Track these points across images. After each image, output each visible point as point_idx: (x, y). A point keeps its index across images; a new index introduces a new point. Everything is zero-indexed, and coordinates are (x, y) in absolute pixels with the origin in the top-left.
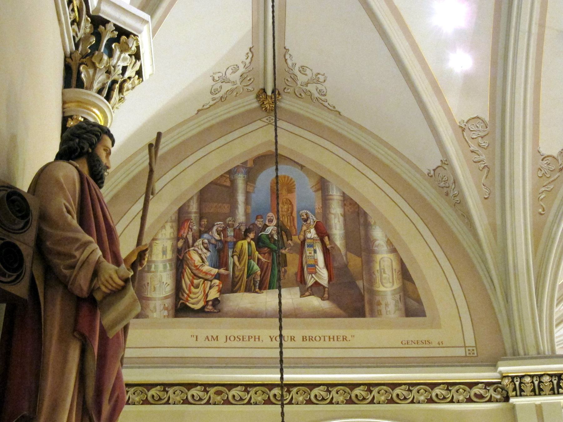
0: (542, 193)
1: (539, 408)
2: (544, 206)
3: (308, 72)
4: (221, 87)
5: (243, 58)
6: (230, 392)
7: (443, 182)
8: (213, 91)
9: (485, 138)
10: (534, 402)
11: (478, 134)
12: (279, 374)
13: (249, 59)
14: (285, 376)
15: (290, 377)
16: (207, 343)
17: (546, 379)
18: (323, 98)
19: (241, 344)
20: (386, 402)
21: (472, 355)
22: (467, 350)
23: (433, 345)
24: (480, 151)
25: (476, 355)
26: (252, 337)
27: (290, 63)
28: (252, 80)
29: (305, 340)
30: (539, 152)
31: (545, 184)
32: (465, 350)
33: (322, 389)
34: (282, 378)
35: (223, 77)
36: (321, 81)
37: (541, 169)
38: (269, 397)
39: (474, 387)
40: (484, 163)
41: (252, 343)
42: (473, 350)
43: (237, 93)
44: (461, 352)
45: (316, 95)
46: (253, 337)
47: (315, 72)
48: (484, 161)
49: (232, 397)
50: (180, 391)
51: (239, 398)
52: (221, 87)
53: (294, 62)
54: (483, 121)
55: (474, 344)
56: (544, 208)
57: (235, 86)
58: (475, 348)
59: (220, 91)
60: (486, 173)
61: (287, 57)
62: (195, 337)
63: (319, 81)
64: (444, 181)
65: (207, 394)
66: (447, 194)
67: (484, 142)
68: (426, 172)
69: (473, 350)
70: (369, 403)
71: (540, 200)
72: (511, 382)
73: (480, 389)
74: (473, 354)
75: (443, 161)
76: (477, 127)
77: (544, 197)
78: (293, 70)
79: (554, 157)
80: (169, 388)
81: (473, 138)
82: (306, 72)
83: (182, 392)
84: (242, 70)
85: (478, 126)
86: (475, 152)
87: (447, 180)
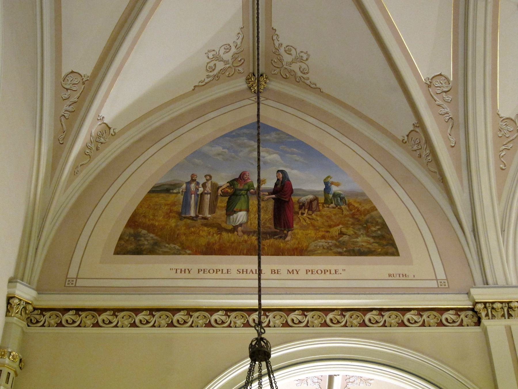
0: (502, 151)
2: (506, 163)
3: (293, 52)
4: (215, 65)
6: (212, 317)
7: (416, 145)
13: (240, 40)
14: (263, 301)
15: (267, 302)
18: (304, 76)
20: (358, 326)
21: (443, 287)
22: (439, 283)
24: (445, 105)
25: (447, 286)
26: (220, 270)
28: (243, 61)
29: (273, 273)
30: (499, 115)
31: (504, 144)
32: (437, 282)
34: (260, 304)
36: (304, 60)
37: (501, 130)
39: (446, 313)
40: (449, 115)
42: (445, 282)
43: (229, 74)
44: (434, 284)
49: (66, 322)
51: (221, 321)
52: (215, 65)
53: (280, 42)
54: (446, 78)
55: (445, 278)
56: (505, 164)
57: (228, 66)
58: (446, 281)
60: (451, 124)
61: (275, 38)
64: (417, 144)
66: (420, 156)
68: (401, 138)
71: (501, 157)
74: (445, 285)
75: (415, 124)
76: (441, 83)
77: (505, 154)
78: (280, 50)
79: (512, 119)
80: (155, 312)
82: (291, 52)
83: (168, 317)
84: (233, 50)
87: (420, 142)
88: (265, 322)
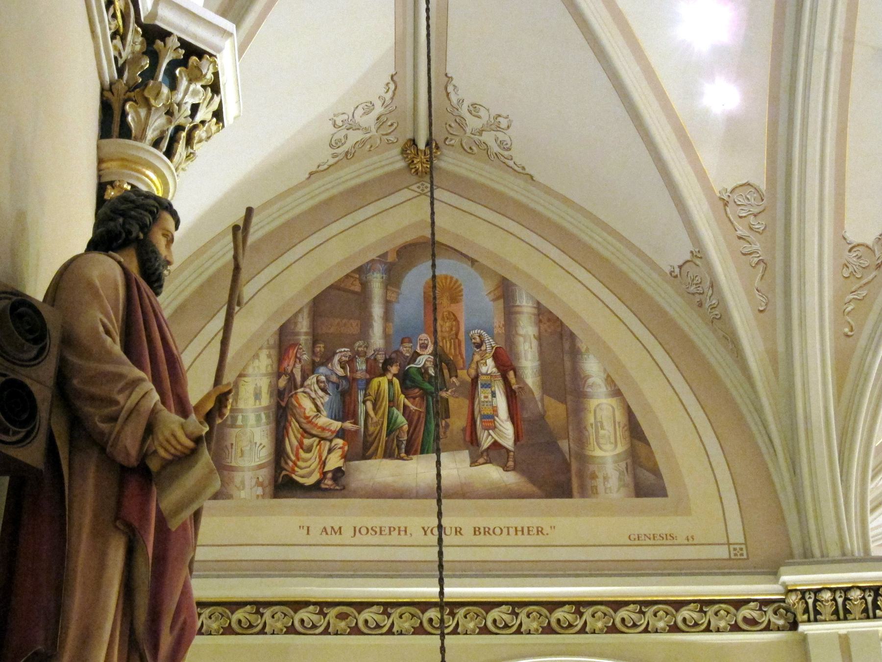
0: (849, 302)
1: (844, 640)
2: (852, 323)
3: (483, 113)
4: (346, 137)
5: (381, 91)
6: (360, 615)
7: (695, 286)
8: (333, 143)
9: (760, 216)
10: (837, 631)
11: (749, 211)
12: (437, 587)
13: (390, 93)
14: (446, 590)
15: (455, 591)
16: (325, 539)
17: (856, 594)
18: (506, 153)
19: (377, 539)
21: (739, 557)
22: (732, 549)
23: (679, 541)
24: (752, 237)
25: (745, 557)
26: (395, 529)
27: (454, 98)
28: (395, 125)
29: (477, 533)
30: (845, 239)
31: (853, 289)
32: (729, 548)
33: (505, 611)
34: (441, 593)
35: (349, 120)
36: (503, 127)
37: (848, 265)
38: (421, 623)
39: (743, 608)
40: (758, 255)
41: (394, 538)
42: (741, 549)
43: (371, 147)
44: (722, 552)
45: (495, 149)
46: (397, 529)
47: (493, 113)
48: (758, 253)
49: (364, 623)
50: (283, 613)
51: (375, 624)
52: (346, 137)
53: (460, 97)
54: (757, 190)
55: (742, 540)
56: (852, 327)
57: (368, 135)
58: (743, 547)
59: (345, 142)
60: (761, 272)
61: (450, 89)
62: (306, 528)
63: (500, 128)
64: (696, 284)
65: (324, 618)
66: (700, 305)
67: (759, 223)
68: (667, 270)
69: (741, 549)
70: (578, 632)
71: (845, 314)
72: (800, 599)
73: (752, 610)
74: (742, 555)
75: (694, 253)
76: (748, 199)
77: (852, 309)
78: (460, 110)
79: (867, 247)
80: (264, 608)
81: (741, 217)
82: (479, 114)
83: (285, 615)
84: (379, 110)
85: (750, 198)
86: (744, 239)
87: (701, 283)
88: (321, 626)
